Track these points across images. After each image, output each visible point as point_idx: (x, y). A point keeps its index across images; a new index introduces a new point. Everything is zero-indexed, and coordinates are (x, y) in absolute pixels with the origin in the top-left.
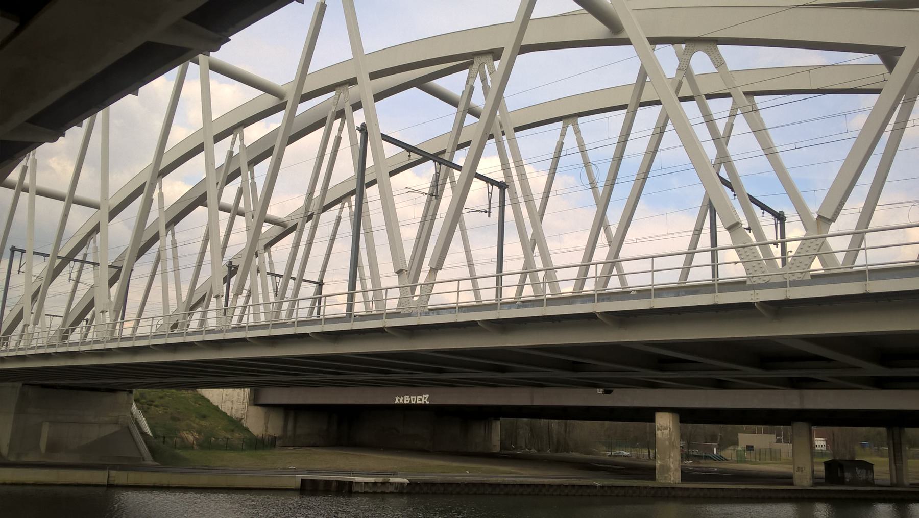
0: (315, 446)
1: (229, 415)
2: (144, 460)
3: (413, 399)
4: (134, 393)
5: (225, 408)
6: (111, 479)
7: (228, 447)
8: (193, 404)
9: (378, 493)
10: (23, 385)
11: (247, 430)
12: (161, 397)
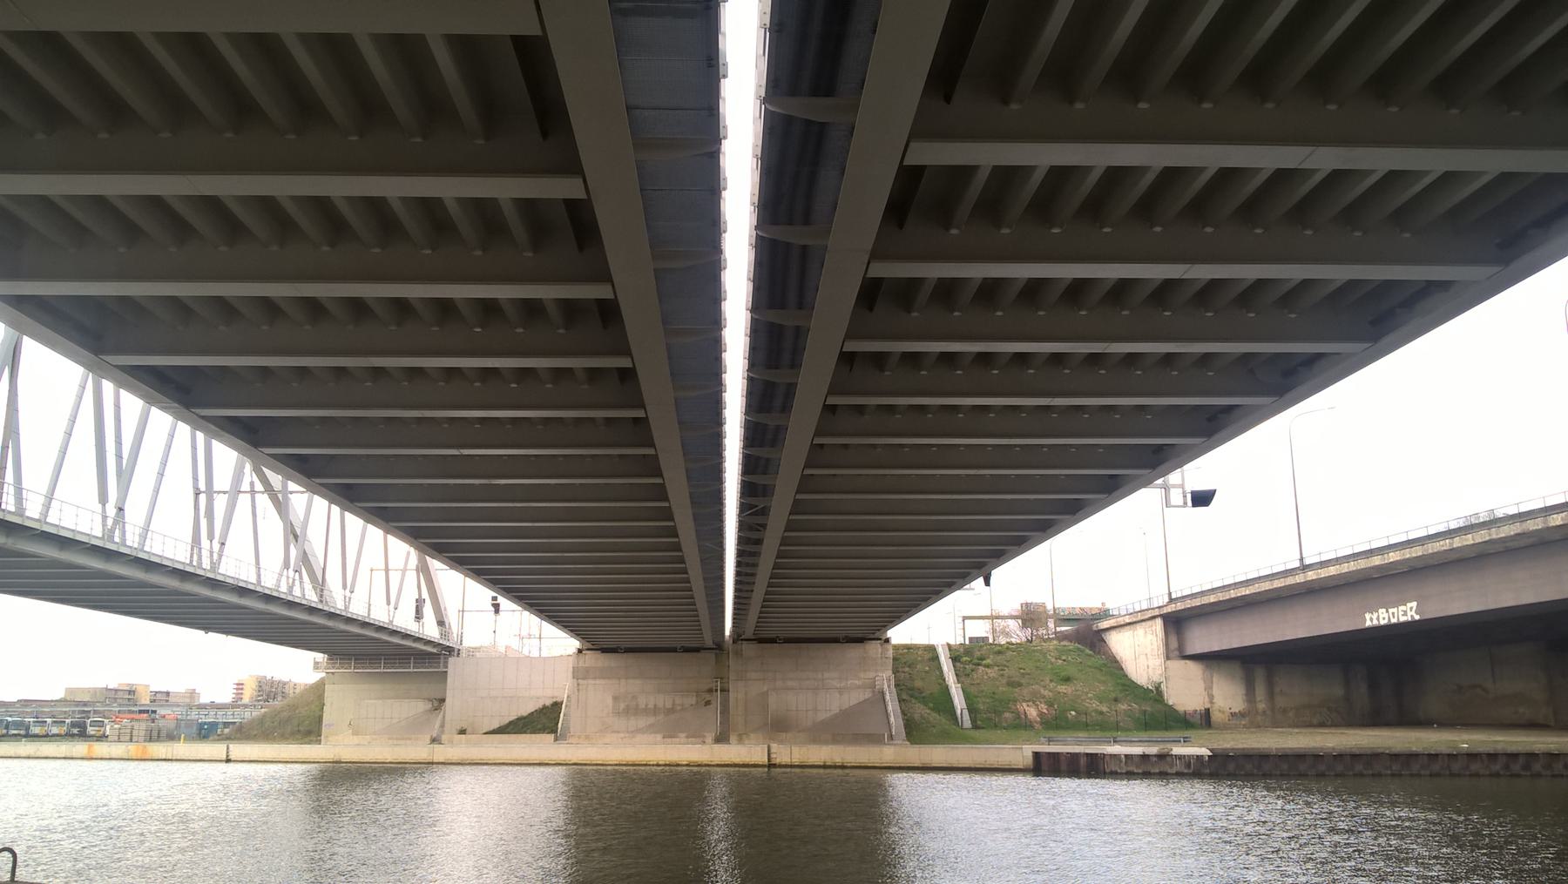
3: (1393, 614)
6: (773, 756)
8: (1053, 660)
9: (1154, 774)
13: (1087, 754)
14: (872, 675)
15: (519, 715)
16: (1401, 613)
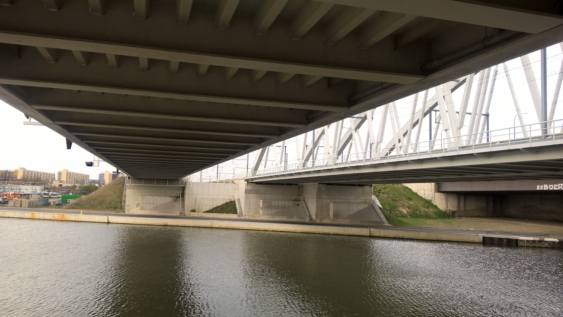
0: (479, 217)
1: (423, 198)
2: (384, 223)
4: (373, 186)
5: (421, 194)
7: (427, 216)
10: (318, 183)
11: (436, 207)
12: (385, 188)
13: (507, 238)
14: (365, 198)
15: (217, 205)
16: (554, 187)
